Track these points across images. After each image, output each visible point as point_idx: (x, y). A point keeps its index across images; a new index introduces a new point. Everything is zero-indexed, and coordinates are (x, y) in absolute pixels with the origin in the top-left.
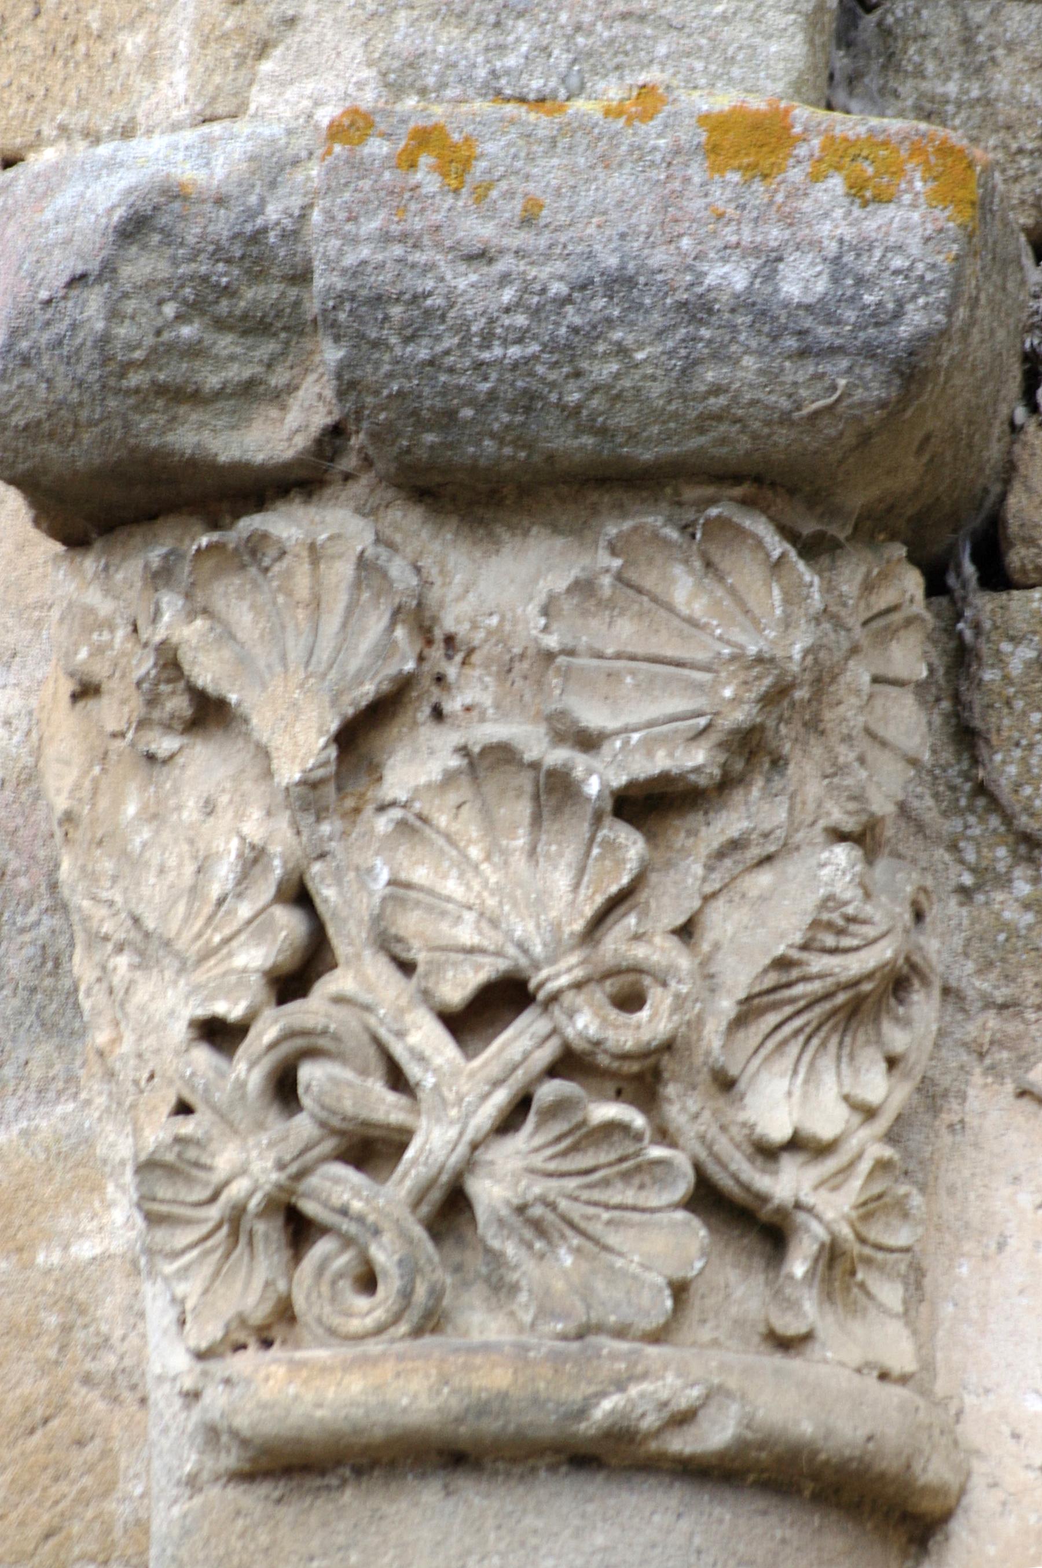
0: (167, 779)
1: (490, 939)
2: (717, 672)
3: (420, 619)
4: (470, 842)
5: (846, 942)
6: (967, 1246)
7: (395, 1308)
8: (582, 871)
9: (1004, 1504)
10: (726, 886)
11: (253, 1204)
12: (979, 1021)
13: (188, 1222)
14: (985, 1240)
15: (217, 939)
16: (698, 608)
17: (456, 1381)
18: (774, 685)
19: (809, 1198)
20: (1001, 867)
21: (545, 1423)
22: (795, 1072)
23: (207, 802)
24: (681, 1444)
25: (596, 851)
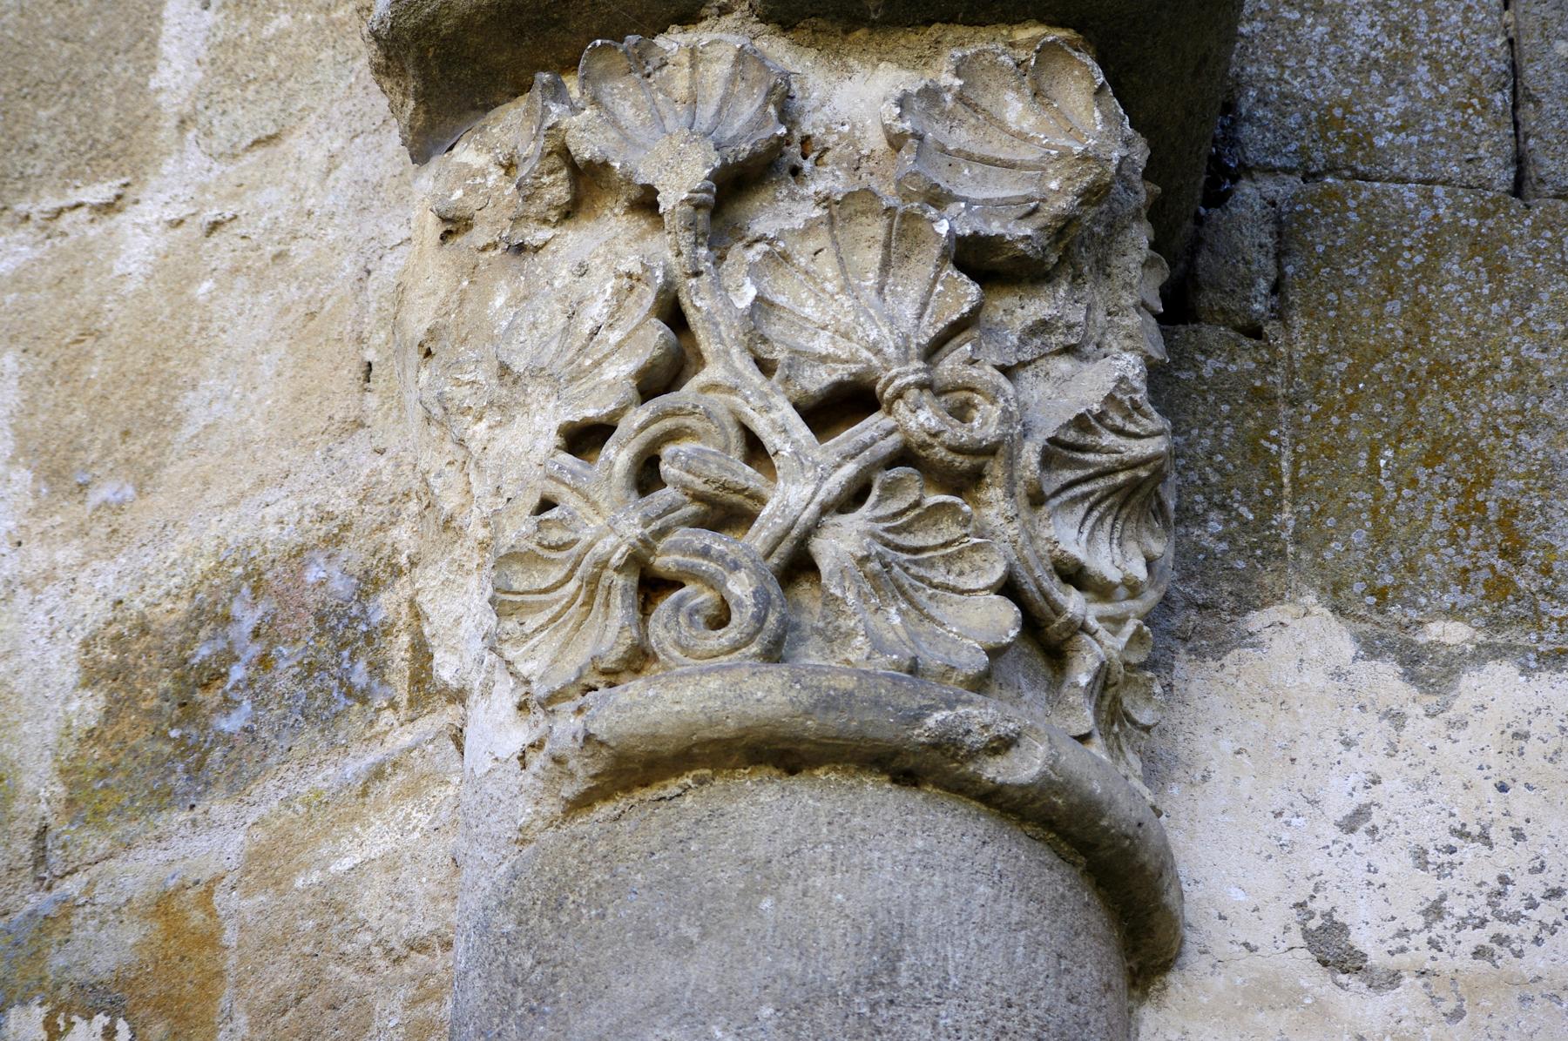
0: (535, 265)
1: (843, 349)
2: (1044, 169)
3: (784, 103)
4: (825, 279)
5: (1131, 427)
6: (1178, 774)
7: (750, 630)
8: (924, 305)
9: (1214, 966)
10: (1034, 361)
11: (616, 559)
12: (1183, 616)
13: (541, 607)
14: (1192, 772)
15: (588, 362)
16: (1028, 124)
17: (807, 680)
18: (1094, 182)
19: (1093, 623)
20: (1199, 509)
21: (884, 727)
22: (1082, 523)
23: (581, 265)
24: (994, 771)
25: (939, 288)
